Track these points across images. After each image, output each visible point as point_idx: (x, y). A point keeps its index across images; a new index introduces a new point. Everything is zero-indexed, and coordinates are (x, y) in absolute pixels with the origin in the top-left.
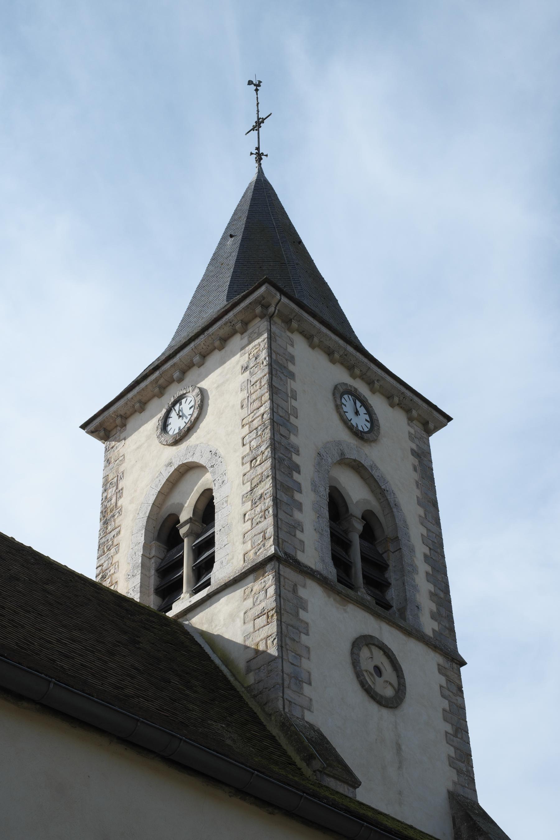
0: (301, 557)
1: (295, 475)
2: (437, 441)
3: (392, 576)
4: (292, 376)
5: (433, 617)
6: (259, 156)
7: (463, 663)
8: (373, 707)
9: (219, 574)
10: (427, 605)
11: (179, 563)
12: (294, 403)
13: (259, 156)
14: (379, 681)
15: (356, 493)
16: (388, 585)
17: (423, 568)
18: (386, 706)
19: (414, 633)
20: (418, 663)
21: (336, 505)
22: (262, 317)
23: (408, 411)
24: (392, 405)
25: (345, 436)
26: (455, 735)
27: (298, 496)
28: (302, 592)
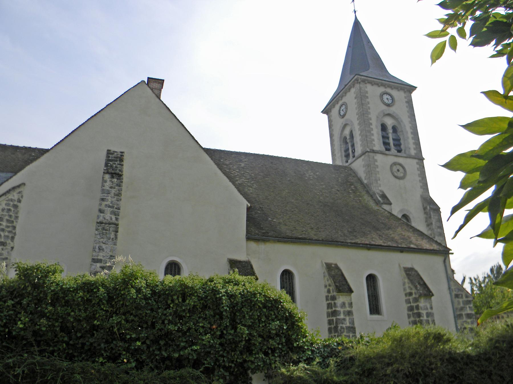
0: (375, 148)
1: (371, 126)
2: (414, 95)
3: (402, 142)
4: (367, 97)
5: (415, 149)
6: (355, 12)
7: (424, 159)
8: (397, 180)
9: (356, 154)
10: (412, 146)
11: (348, 149)
12: (369, 105)
13: (355, 12)
14: (399, 173)
15: (389, 122)
16: (401, 144)
17: (410, 136)
18: (401, 179)
19: (409, 157)
20: (410, 164)
21: (384, 127)
22: (357, 83)
23: (404, 90)
24: (399, 90)
25: (385, 107)
26: (422, 180)
27: (372, 132)
28: (375, 158)
